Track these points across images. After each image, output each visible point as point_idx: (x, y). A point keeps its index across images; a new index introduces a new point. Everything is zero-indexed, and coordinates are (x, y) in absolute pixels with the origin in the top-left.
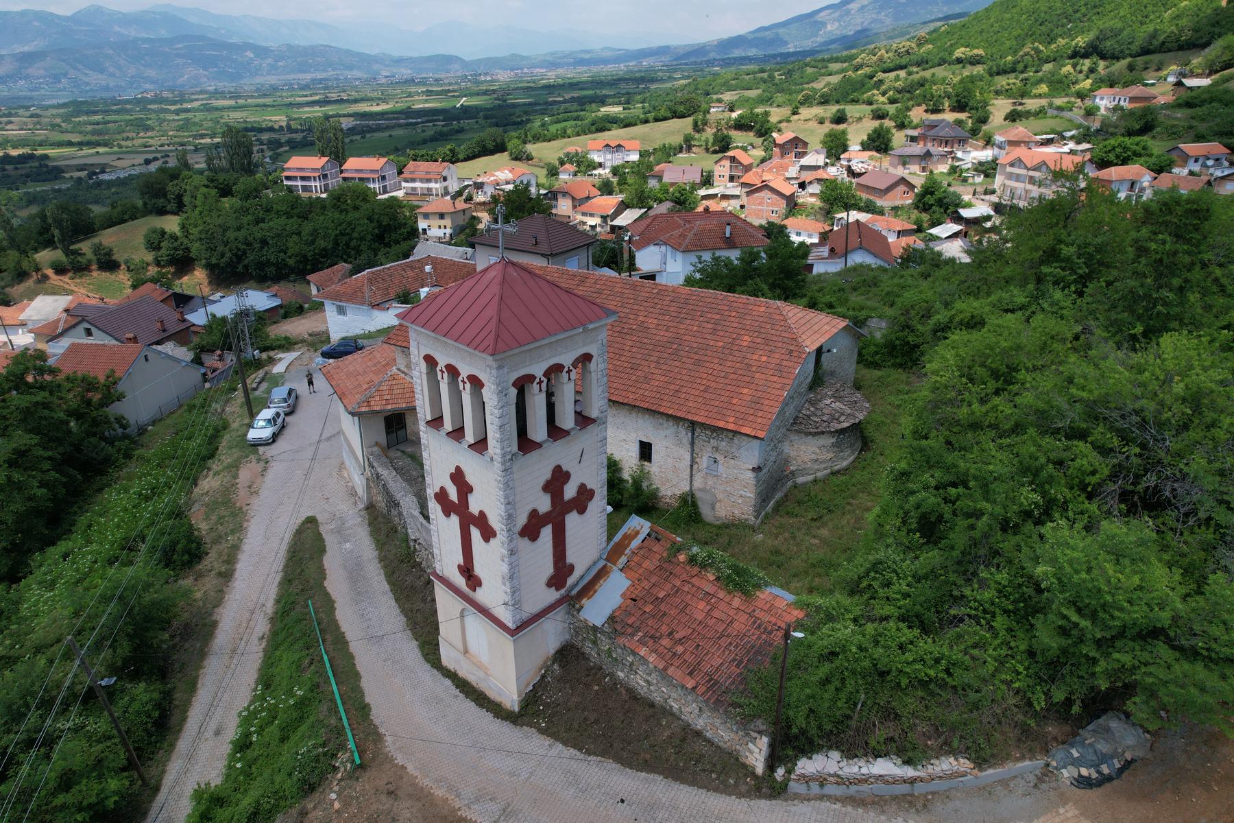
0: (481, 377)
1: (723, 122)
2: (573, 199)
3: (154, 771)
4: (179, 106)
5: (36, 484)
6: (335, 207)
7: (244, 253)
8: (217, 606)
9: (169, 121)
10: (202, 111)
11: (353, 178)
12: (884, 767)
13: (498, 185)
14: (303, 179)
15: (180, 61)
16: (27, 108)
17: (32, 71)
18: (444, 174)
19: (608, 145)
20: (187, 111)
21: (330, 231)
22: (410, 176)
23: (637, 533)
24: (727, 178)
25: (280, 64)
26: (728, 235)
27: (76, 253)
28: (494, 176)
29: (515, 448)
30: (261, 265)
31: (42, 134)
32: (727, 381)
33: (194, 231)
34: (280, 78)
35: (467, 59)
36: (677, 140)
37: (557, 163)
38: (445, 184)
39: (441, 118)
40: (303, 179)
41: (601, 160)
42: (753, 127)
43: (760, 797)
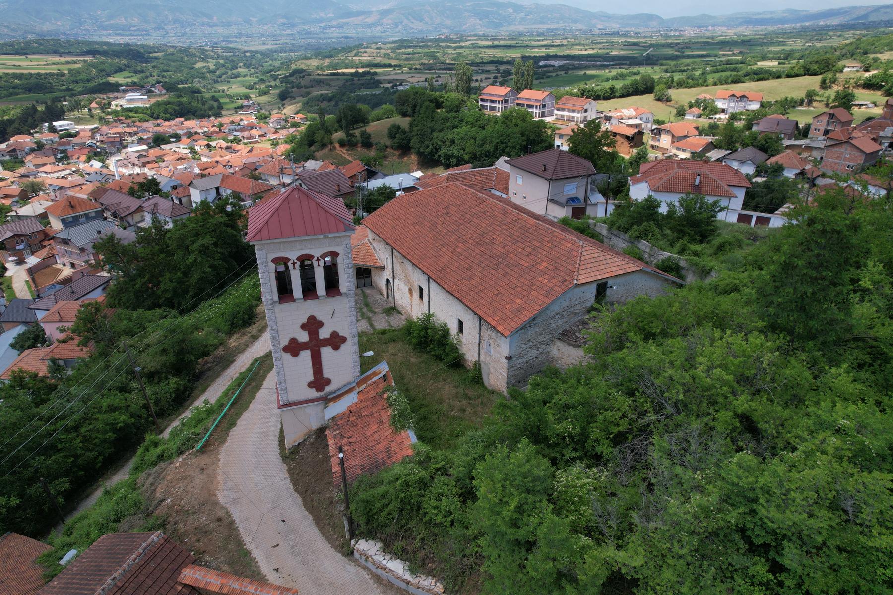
0: (310, 253)
1: (852, 81)
2: (673, 136)
3: (165, 423)
4: (458, 44)
5: (207, 265)
6: (503, 123)
7: (440, 148)
8: (240, 353)
9: (449, 53)
10: (470, 48)
11: (524, 104)
12: (397, 566)
13: (622, 119)
14: (492, 101)
15: (467, 14)
16: (376, 43)
17: (385, 21)
18: (586, 107)
19: (733, 95)
20: (461, 47)
21: (494, 139)
22: (561, 106)
23: (380, 373)
24: (822, 131)
25: (529, 17)
26: (697, 183)
27: (352, 135)
28: (621, 112)
29: (276, 298)
30: (448, 157)
31: (378, 60)
32: (513, 292)
33: (415, 129)
34: (527, 27)
35: (664, 18)
36: (800, 94)
37: (686, 106)
38: (585, 114)
39: (628, 62)
40: (492, 101)
41: (725, 107)
42: (882, 86)
43: (340, 552)
